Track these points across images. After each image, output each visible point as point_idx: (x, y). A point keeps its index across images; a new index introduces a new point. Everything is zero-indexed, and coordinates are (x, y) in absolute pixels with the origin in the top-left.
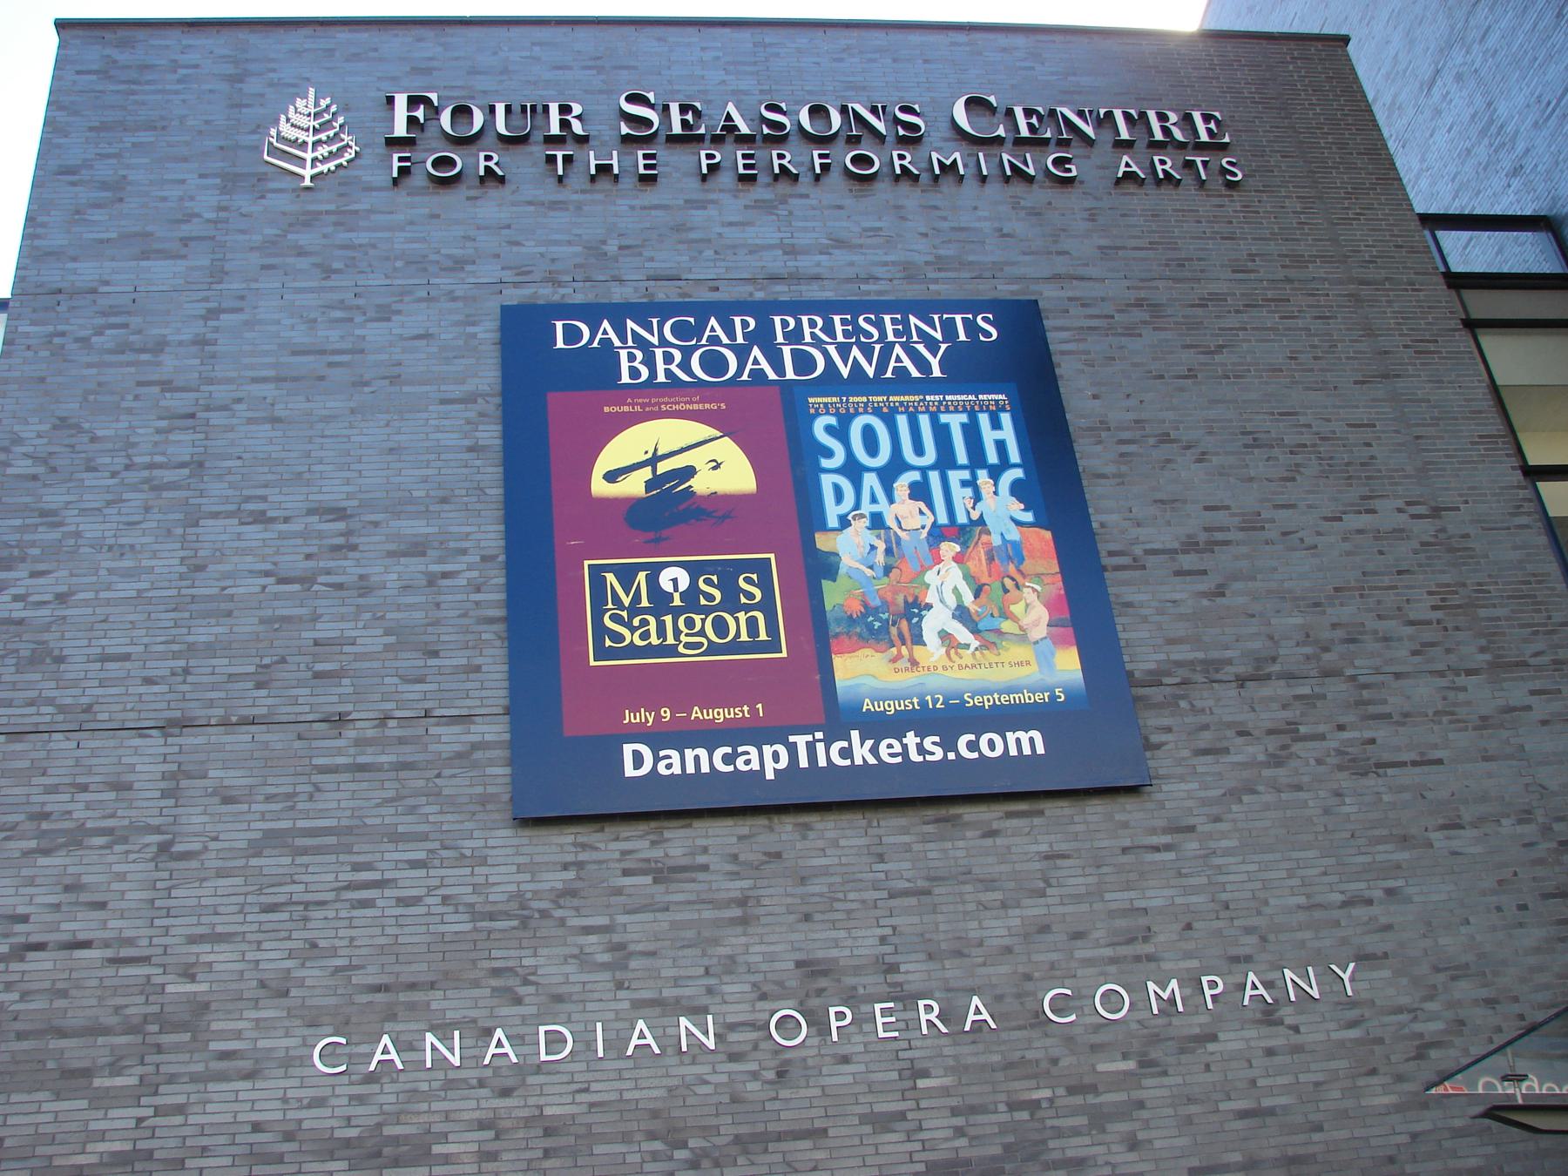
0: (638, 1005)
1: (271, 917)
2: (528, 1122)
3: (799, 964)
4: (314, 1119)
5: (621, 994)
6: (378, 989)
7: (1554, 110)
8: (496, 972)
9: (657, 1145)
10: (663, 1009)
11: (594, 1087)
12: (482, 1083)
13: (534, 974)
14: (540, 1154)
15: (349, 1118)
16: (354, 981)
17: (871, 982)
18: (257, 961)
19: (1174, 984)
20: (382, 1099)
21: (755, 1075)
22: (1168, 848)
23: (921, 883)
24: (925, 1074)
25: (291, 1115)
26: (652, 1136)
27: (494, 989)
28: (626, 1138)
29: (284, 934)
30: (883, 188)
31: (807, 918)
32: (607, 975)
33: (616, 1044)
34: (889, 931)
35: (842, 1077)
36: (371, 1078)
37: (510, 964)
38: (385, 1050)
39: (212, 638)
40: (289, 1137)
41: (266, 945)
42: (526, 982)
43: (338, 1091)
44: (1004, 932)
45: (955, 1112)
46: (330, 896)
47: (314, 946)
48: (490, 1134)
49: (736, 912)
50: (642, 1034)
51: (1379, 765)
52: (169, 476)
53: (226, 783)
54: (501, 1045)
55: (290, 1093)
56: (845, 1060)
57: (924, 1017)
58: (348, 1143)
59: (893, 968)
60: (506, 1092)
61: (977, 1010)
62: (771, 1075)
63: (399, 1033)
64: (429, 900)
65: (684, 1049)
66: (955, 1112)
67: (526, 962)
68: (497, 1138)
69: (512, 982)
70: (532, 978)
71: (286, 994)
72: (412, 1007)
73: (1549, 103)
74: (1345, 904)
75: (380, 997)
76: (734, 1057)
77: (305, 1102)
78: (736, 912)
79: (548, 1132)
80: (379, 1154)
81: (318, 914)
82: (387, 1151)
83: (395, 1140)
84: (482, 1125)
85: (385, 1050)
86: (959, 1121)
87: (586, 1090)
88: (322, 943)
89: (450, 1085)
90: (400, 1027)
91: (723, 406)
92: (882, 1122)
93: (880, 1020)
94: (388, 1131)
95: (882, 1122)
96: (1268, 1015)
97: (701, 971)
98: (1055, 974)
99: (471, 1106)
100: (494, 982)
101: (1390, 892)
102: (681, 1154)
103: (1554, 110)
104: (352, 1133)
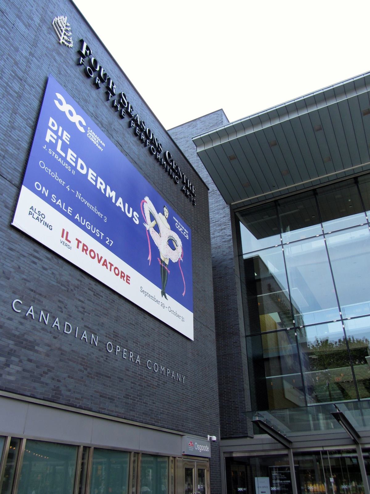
1: (10, 252)
7: (213, 223)
10: (91, 331)
12: (51, 333)
16: (27, 285)
18: (3, 264)
29: (12, 259)
30: (89, 81)
38: (31, 311)
39: (13, 153)
41: (7, 260)
44: (4, 9)
46: (26, 255)
47: (19, 268)
52: (12, 92)
53: (7, 201)
64: (49, 271)
71: (8, 279)
73: (213, 221)
81: (22, 258)
88: (22, 269)
91: (102, 150)
94: (26, 336)
103: (213, 223)
104: (17, 333)
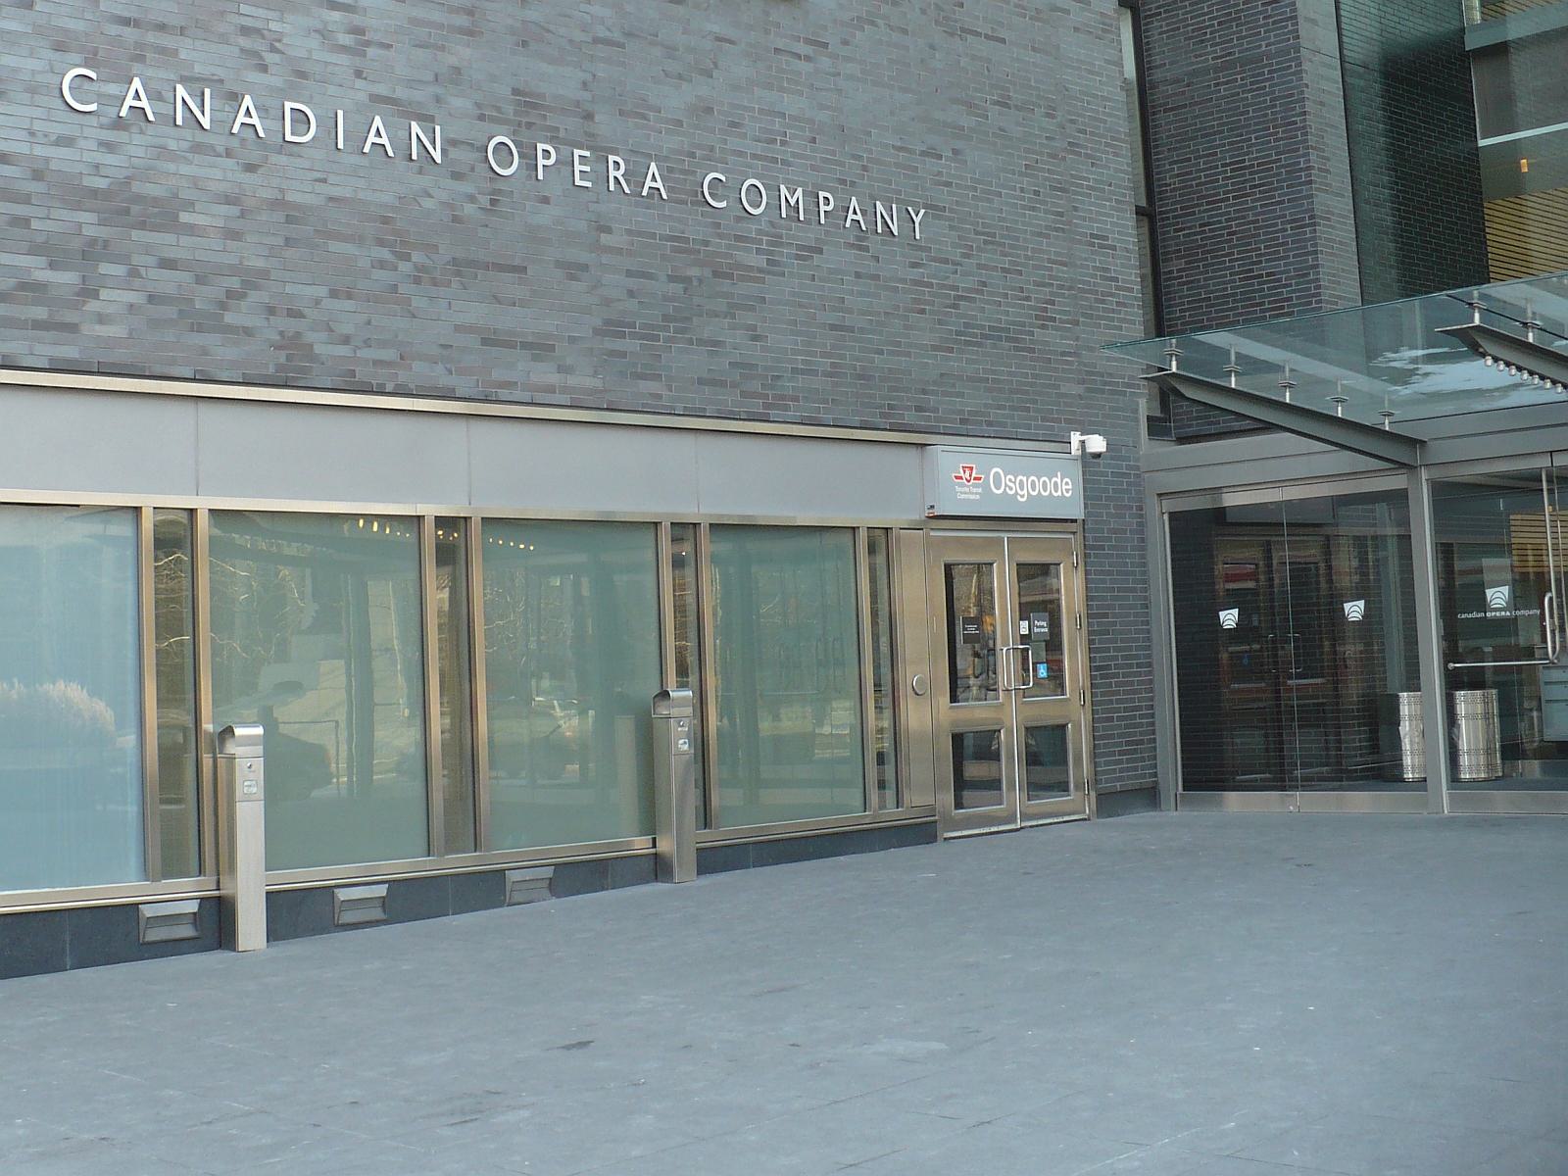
0: (376, 99)
2: (278, 204)
3: (516, 92)
4: (60, 158)
5: (359, 83)
6: (126, 22)
8: (245, 31)
9: (385, 254)
11: (332, 179)
12: (229, 153)
13: (280, 41)
14: (281, 241)
15: (97, 166)
17: (569, 124)
19: (799, 192)
20: (133, 151)
21: (472, 199)
22: (808, 58)
23: (616, 36)
24: (608, 230)
25: (38, 151)
26: (381, 243)
27: (242, 50)
28: (359, 239)
31: (525, 44)
32: (343, 59)
33: (357, 138)
34: (589, 77)
35: (545, 216)
36: (119, 124)
37: (259, 25)
38: (135, 94)
40: (37, 175)
42: (273, 50)
43: (87, 132)
45: (629, 274)
48: (235, 210)
49: (462, 21)
50: (378, 132)
51: (963, 30)
54: (248, 113)
55: (37, 126)
56: (546, 200)
57: (612, 173)
58: (94, 193)
59: (589, 116)
60: (250, 168)
61: (653, 179)
62: (484, 201)
63: (151, 78)
65: (414, 157)
66: (629, 274)
67: (273, 26)
68: (242, 215)
69: (259, 45)
70: (277, 44)
72: (162, 50)
74: (923, 153)
75: (129, 33)
76: (457, 176)
77: (53, 138)
78: (462, 21)
79: (289, 220)
80: (127, 212)
82: (135, 209)
83: (139, 199)
84: (228, 200)
85: (135, 94)
86: (633, 283)
87: (324, 181)
89: (197, 148)
90: (150, 72)
92: (574, 270)
93: (578, 167)
95: (574, 270)
96: (860, 239)
97: (431, 78)
98: (712, 160)
99: (221, 174)
100: (243, 42)
101: (955, 152)
102: (405, 267)
104: (101, 183)
